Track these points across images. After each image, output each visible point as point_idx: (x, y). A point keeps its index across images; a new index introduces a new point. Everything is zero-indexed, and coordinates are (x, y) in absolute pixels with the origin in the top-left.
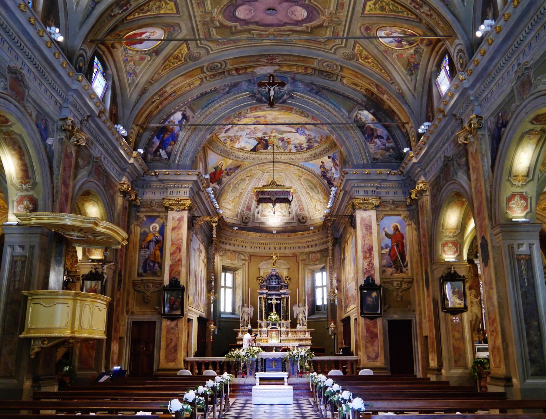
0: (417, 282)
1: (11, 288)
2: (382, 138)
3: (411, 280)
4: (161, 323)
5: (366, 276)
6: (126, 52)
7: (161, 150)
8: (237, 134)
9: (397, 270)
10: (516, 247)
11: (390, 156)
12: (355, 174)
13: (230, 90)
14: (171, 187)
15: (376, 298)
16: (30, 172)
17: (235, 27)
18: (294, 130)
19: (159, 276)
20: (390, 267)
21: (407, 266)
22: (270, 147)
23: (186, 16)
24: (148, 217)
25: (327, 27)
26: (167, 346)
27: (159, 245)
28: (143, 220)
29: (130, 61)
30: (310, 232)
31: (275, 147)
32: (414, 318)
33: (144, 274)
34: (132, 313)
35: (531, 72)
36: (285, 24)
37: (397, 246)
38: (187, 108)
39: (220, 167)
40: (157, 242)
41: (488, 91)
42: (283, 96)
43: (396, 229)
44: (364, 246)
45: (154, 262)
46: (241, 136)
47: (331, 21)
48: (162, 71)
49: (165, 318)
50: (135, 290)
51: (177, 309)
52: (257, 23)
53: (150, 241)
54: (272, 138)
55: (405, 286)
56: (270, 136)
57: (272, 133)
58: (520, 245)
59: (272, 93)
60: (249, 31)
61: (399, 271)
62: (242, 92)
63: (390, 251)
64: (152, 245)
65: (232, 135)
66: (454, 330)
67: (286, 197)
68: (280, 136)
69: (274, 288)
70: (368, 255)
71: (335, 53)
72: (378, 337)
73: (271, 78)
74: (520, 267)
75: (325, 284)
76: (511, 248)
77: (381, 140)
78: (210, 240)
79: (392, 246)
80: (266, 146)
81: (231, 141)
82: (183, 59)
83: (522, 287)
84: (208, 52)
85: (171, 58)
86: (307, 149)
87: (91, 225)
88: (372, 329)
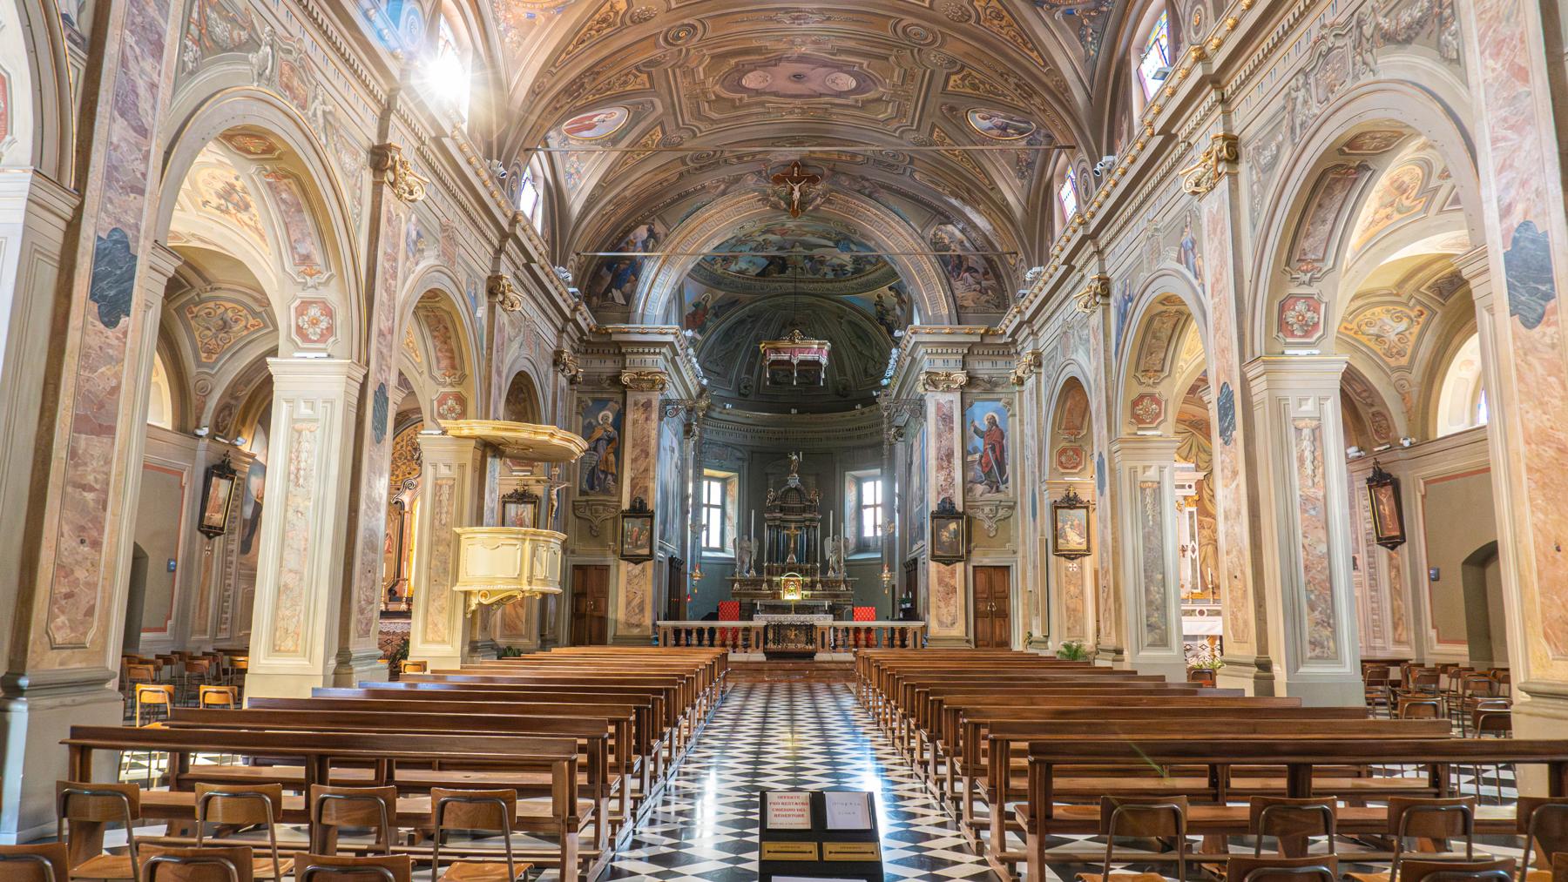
0: (1022, 508)
1: (437, 523)
2: (976, 271)
4: (618, 566)
5: (941, 497)
10: (1140, 471)
11: (987, 302)
13: (727, 188)
14: (632, 353)
15: (956, 533)
16: (457, 361)
17: (741, 100)
18: (831, 244)
20: (981, 483)
23: (664, 91)
24: (595, 400)
25: (888, 102)
26: (628, 603)
27: (613, 445)
28: (587, 406)
34: (573, 552)
35: (1161, 235)
36: (821, 95)
37: (993, 449)
40: (610, 440)
42: (814, 199)
43: (993, 422)
44: (939, 449)
47: (895, 94)
51: (642, 547)
52: (776, 94)
53: (598, 440)
55: (1001, 513)
58: (1145, 468)
59: (797, 194)
60: (762, 104)
62: (748, 193)
63: (981, 457)
66: (1068, 582)
68: (807, 253)
69: (791, 511)
70: (945, 464)
71: (901, 137)
74: (1143, 500)
75: (879, 501)
76: (1133, 471)
83: (1144, 528)
84: (695, 135)
87: (546, 438)
88: (947, 580)
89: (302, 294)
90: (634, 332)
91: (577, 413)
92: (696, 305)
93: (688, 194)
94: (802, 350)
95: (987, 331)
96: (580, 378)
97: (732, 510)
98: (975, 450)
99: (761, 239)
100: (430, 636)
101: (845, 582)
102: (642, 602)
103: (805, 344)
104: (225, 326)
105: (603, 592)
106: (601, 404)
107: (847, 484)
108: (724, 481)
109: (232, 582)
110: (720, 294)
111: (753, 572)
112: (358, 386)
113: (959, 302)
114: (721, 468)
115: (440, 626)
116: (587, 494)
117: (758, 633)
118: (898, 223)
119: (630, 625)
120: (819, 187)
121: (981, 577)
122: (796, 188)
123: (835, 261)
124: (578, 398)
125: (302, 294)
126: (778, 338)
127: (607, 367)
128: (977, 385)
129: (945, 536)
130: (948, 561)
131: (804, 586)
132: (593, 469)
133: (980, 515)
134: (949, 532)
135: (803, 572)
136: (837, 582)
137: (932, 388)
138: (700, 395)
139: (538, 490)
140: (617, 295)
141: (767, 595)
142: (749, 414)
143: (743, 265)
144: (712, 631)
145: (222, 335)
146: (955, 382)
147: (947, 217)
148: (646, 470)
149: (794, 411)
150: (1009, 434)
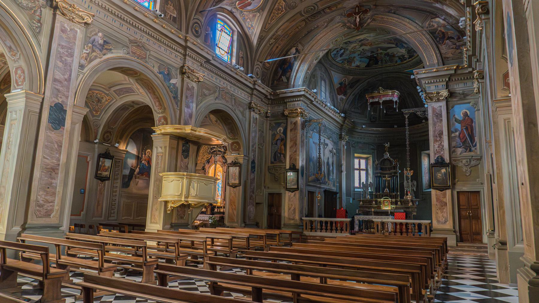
2: (453, 38)
3: (480, 157)
5: (437, 156)
6: (242, 13)
7: (283, 77)
8: (351, 56)
9: (467, 149)
12: (425, 73)
14: (289, 102)
15: (445, 174)
16: (161, 102)
18: (394, 46)
19: (283, 163)
20: (460, 147)
21: (476, 145)
22: (380, 62)
24: (275, 123)
26: (289, 209)
29: (247, 19)
32: (482, 190)
33: (274, 162)
34: (268, 188)
37: (467, 129)
38: (299, 44)
39: (344, 82)
40: (282, 140)
43: (466, 114)
44: (434, 131)
45: (280, 154)
46: (354, 57)
48: (271, 22)
49: (287, 190)
50: (270, 173)
53: (278, 140)
54: (379, 54)
55: (473, 163)
59: (358, 20)
61: (468, 151)
63: (460, 134)
64: (279, 142)
67: (391, 99)
68: (385, 52)
70: (438, 139)
72: (447, 205)
73: (357, 8)
77: (452, 40)
79: (462, 130)
80: (377, 63)
81: (348, 62)
82: (284, 10)
85: (274, 11)
88: (442, 199)
89: (15, 65)
90: (288, 92)
91: (270, 129)
92: (341, 84)
93: (312, 30)
94: (384, 96)
95: (458, 67)
96: (269, 115)
97: (370, 171)
98: (456, 130)
99: (361, 49)
100: (153, 220)
102: (295, 209)
103: (385, 93)
104: (99, 101)
105: (279, 206)
106: (279, 125)
107: (422, 157)
108: (367, 159)
109: (117, 198)
110: (351, 77)
112: (40, 104)
113: (444, 56)
115: (156, 216)
116: (273, 163)
117: (346, 224)
118: (409, 23)
119: (290, 219)
120: (369, 14)
121: (463, 198)
122: (358, 17)
123: (400, 54)
124: (270, 123)
125: (15, 65)
126: (372, 93)
127: (279, 109)
128: (455, 97)
129: (439, 175)
130: (442, 189)
131: (392, 203)
132: (276, 152)
133: (460, 164)
134: (441, 173)
135: (391, 197)
137: (429, 101)
138: (344, 122)
139: (241, 161)
140: (284, 79)
143: (357, 63)
144: (332, 223)
145: (99, 104)
146: (442, 96)
147: (436, 15)
148: (296, 151)
149: (395, 126)
150: (476, 120)
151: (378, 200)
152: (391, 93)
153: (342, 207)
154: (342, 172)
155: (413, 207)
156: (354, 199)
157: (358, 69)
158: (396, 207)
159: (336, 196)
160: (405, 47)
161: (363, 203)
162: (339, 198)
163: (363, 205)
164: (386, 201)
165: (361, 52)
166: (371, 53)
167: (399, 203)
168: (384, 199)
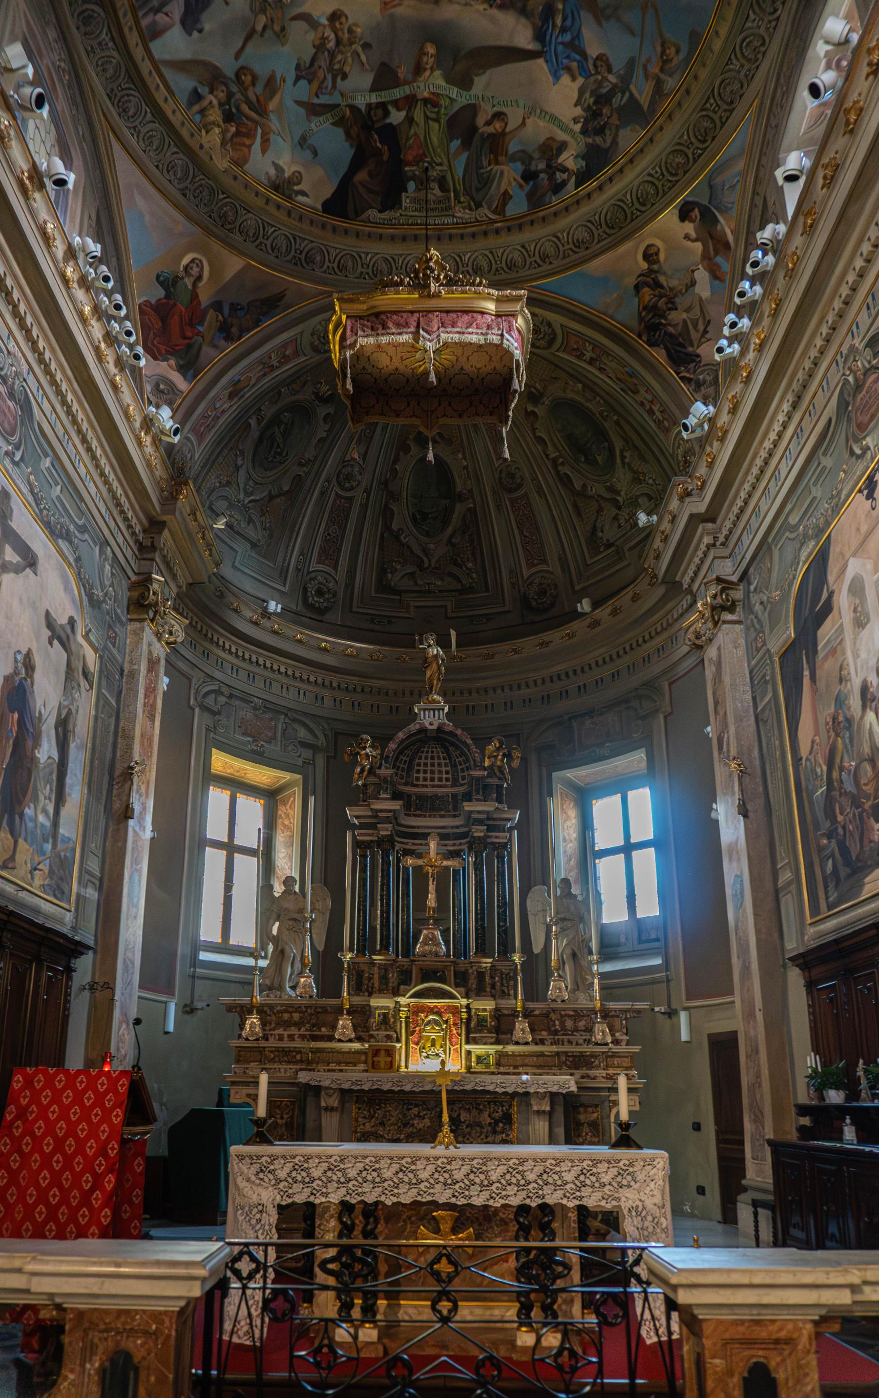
22: (411, 186)
30: (576, 626)
31: (436, 191)
39: (189, 282)
41: (666, 635)
56: (410, 101)
57: (418, 70)
65: (228, 65)
68: (459, 97)
78: (136, 594)
86: (582, 177)
101: (606, 1014)
110: (234, 264)
111: (308, 981)
114: (258, 757)
136: (578, 1015)
138: (170, 499)
141: (350, 1059)
142: (326, 640)
151: (375, 1002)
152: (491, 306)
153: (106, 1057)
154: (127, 813)
155: (615, 1055)
156: (188, 1009)
157: (279, 207)
158: (500, 1055)
159: (69, 971)
160: (584, 55)
161: (264, 1024)
162: (92, 987)
163: (266, 1038)
164: (431, 1011)
165: (320, 47)
166: (373, 89)
167: (521, 1027)
168: (415, 995)
